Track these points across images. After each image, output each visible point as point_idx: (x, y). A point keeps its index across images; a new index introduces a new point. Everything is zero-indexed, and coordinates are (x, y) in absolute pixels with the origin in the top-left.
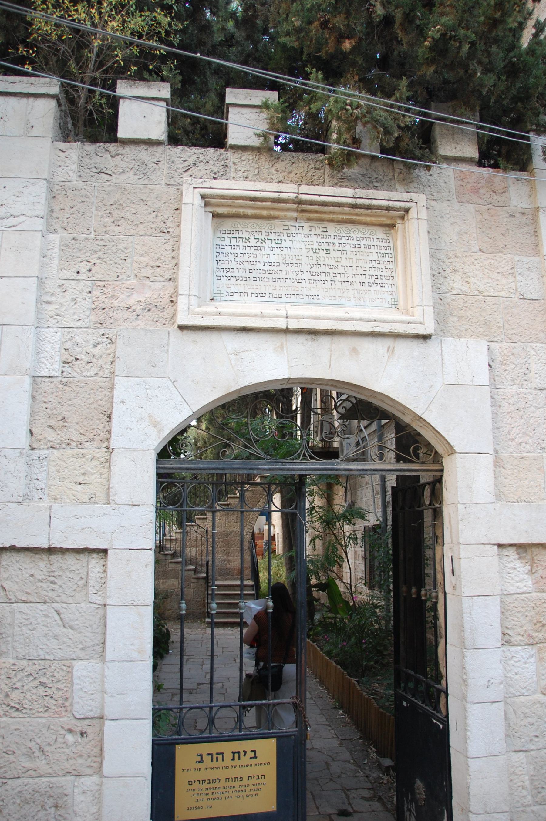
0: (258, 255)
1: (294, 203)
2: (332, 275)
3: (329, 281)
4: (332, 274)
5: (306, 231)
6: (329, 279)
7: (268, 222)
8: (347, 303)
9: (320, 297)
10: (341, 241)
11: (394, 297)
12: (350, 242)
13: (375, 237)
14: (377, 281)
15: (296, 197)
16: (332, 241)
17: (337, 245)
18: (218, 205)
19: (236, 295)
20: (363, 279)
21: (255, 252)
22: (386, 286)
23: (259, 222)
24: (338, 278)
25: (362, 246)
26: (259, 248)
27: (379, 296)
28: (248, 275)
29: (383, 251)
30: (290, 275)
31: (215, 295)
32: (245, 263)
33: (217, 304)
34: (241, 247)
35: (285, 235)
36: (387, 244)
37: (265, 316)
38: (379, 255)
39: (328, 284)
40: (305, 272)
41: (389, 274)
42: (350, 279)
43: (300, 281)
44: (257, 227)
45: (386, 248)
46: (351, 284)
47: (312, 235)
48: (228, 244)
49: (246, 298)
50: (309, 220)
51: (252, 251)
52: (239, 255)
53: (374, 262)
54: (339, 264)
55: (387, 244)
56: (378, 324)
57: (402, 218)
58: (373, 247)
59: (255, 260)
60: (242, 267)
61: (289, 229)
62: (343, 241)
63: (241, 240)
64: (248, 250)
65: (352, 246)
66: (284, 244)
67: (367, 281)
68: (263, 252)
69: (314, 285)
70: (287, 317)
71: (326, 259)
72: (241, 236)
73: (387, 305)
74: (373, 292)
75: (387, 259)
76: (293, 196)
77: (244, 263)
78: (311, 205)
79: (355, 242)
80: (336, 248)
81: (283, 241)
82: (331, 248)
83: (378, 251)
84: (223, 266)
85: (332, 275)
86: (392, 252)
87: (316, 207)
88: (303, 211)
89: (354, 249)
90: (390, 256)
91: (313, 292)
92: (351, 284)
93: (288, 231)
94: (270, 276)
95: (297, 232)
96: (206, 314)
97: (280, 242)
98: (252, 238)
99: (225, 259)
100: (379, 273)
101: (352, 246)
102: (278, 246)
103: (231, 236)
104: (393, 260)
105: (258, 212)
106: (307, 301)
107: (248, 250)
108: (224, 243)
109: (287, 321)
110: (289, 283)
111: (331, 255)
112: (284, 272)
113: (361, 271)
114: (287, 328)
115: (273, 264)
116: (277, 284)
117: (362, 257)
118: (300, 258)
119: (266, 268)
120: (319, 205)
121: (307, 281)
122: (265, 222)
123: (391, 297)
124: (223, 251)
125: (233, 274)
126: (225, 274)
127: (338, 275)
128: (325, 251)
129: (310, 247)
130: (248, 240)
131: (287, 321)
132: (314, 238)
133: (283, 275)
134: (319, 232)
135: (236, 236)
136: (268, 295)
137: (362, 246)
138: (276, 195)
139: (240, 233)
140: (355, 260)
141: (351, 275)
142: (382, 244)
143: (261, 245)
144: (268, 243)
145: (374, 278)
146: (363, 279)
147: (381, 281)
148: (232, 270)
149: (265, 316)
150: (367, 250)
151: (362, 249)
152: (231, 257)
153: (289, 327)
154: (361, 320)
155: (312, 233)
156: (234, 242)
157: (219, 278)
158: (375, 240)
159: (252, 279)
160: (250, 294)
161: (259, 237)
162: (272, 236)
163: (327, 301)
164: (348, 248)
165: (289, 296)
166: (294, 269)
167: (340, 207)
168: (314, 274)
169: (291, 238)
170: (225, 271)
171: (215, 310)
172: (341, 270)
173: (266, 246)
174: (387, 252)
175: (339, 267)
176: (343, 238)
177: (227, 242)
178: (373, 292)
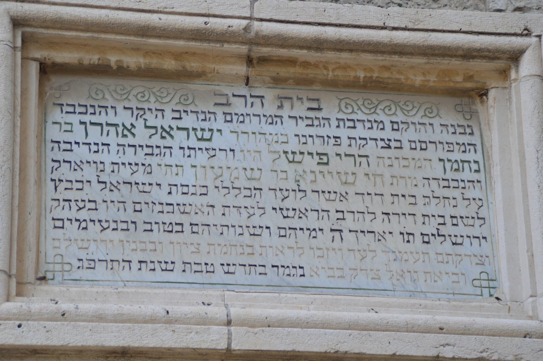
0: (155, 167)
1: (243, 43)
2: (334, 215)
3: (327, 230)
4: (332, 213)
5: (270, 109)
6: (326, 225)
7: (177, 85)
8: (372, 284)
9: (307, 272)
10: (353, 133)
11: (487, 268)
12: (376, 133)
13: (436, 122)
14: (443, 230)
15: (246, 29)
16: (333, 131)
17: (345, 141)
18: (52, 44)
19: (100, 267)
20: (409, 224)
21: (148, 160)
22: (467, 241)
23: (156, 86)
24: (350, 223)
25: (406, 145)
26: (157, 151)
27: (451, 268)
28: (130, 216)
29: (457, 156)
30: (233, 218)
31: (51, 267)
32: (125, 189)
33: (57, 289)
34: (114, 148)
35: (220, 117)
36: (466, 139)
37: (176, 321)
38: (448, 165)
39: (324, 238)
40: (269, 210)
41: (472, 210)
42: (378, 226)
43: (258, 231)
44: (153, 99)
45: (465, 147)
46: (381, 237)
47: (286, 119)
48: (81, 139)
49: (126, 275)
50: (277, 81)
51: (140, 157)
52: (108, 168)
53: (434, 183)
54: (351, 191)
55: (466, 139)
56: (451, 339)
57: (504, 73)
58: (431, 147)
59: (147, 179)
60: (115, 196)
61: (228, 104)
62: (360, 131)
63: (112, 129)
64: (130, 156)
65: (381, 144)
66: (218, 141)
67: (417, 230)
68: (168, 160)
69: (291, 241)
70: (229, 323)
71: (319, 177)
72: (112, 119)
73: (469, 289)
74: (433, 255)
75: (467, 175)
76: (238, 24)
77: (122, 187)
78: (283, 46)
79: (388, 134)
80: (341, 150)
81: (216, 134)
82: (330, 150)
83: (445, 156)
84: (69, 195)
85: (334, 215)
86: (479, 157)
87: (295, 53)
88: (264, 60)
89: (386, 153)
90: (474, 167)
91: (289, 259)
92: (381, 237)
93: (227, 110)
94: (185, 220)
95: (249, 110)
96: (29, 316)
97: (207, 135)
98: (140, 124)
99: (73, 176)
100: (449, 211)
101: (381, 144)
102: (204, 145)
103: (87, 118)
104: (481, 176)
105: (154, 62)
106: (249, 279)
107: (130, 156)
108: (68, 137)
109: (230, 333)
110: (230, 235)
111: (331, 167)
112: (219, 210)
113: (403, 206)
114: (229, 349)
115: (192, 190)
116: (203, 238)
117: (406, 172)
118: (256, 174)
119: (176, 198)
120: (301, 47)
121: (274, 229)
122: (171, 86)
123: (480, 269)
124: (68, 156)
125: (94, 215)
126: (73, 214)
127: (348, 216)
128: (316, 158)
129: (280, 148)
130: (130, 130)
131: (230, 333)
132: (289, 127)
133: (215, 218)
134: (300, 110)
135: (102, 119)
136: (179, 266)
137: (406, 145)
138: (198, 22)
139: (111, 111)
140: (387, 179)
141: (380, 217)
142: (452, 139)
143: (162, 143)
144: (180, 137)
145: (434, 222)
146: (409, 224)
147: (453, 231)
148: (92, 206)
149: (176, 321)
150: (418, 154)
151: (406, 151)
152: (89, 173)
153: (234, 346)
154: (410, 328)
155: (285, 113)
156: (94, 133)
157: (59, 224)
158: (438, 129)
159: (141, 227)
160: (135, 265)
161: (158, 122)
162: (189, 121)
163: (322, 280)
164: (371, 149)
165: (232, 268)
166: (242, 201)
167: (351, 51)
168: (291, 213)
169: (234, 126)
170: (74, 208)
171: (52, 307)
172: (355, 203)
173: (175, 144)
174: (466, 157)
175: (351, 197)
176: (359, 125)
177: (78, 134)
178: (433, 255)
